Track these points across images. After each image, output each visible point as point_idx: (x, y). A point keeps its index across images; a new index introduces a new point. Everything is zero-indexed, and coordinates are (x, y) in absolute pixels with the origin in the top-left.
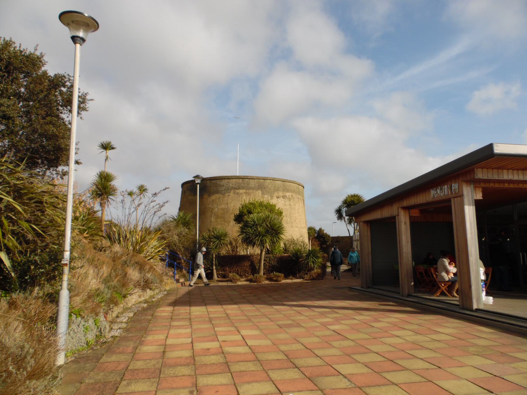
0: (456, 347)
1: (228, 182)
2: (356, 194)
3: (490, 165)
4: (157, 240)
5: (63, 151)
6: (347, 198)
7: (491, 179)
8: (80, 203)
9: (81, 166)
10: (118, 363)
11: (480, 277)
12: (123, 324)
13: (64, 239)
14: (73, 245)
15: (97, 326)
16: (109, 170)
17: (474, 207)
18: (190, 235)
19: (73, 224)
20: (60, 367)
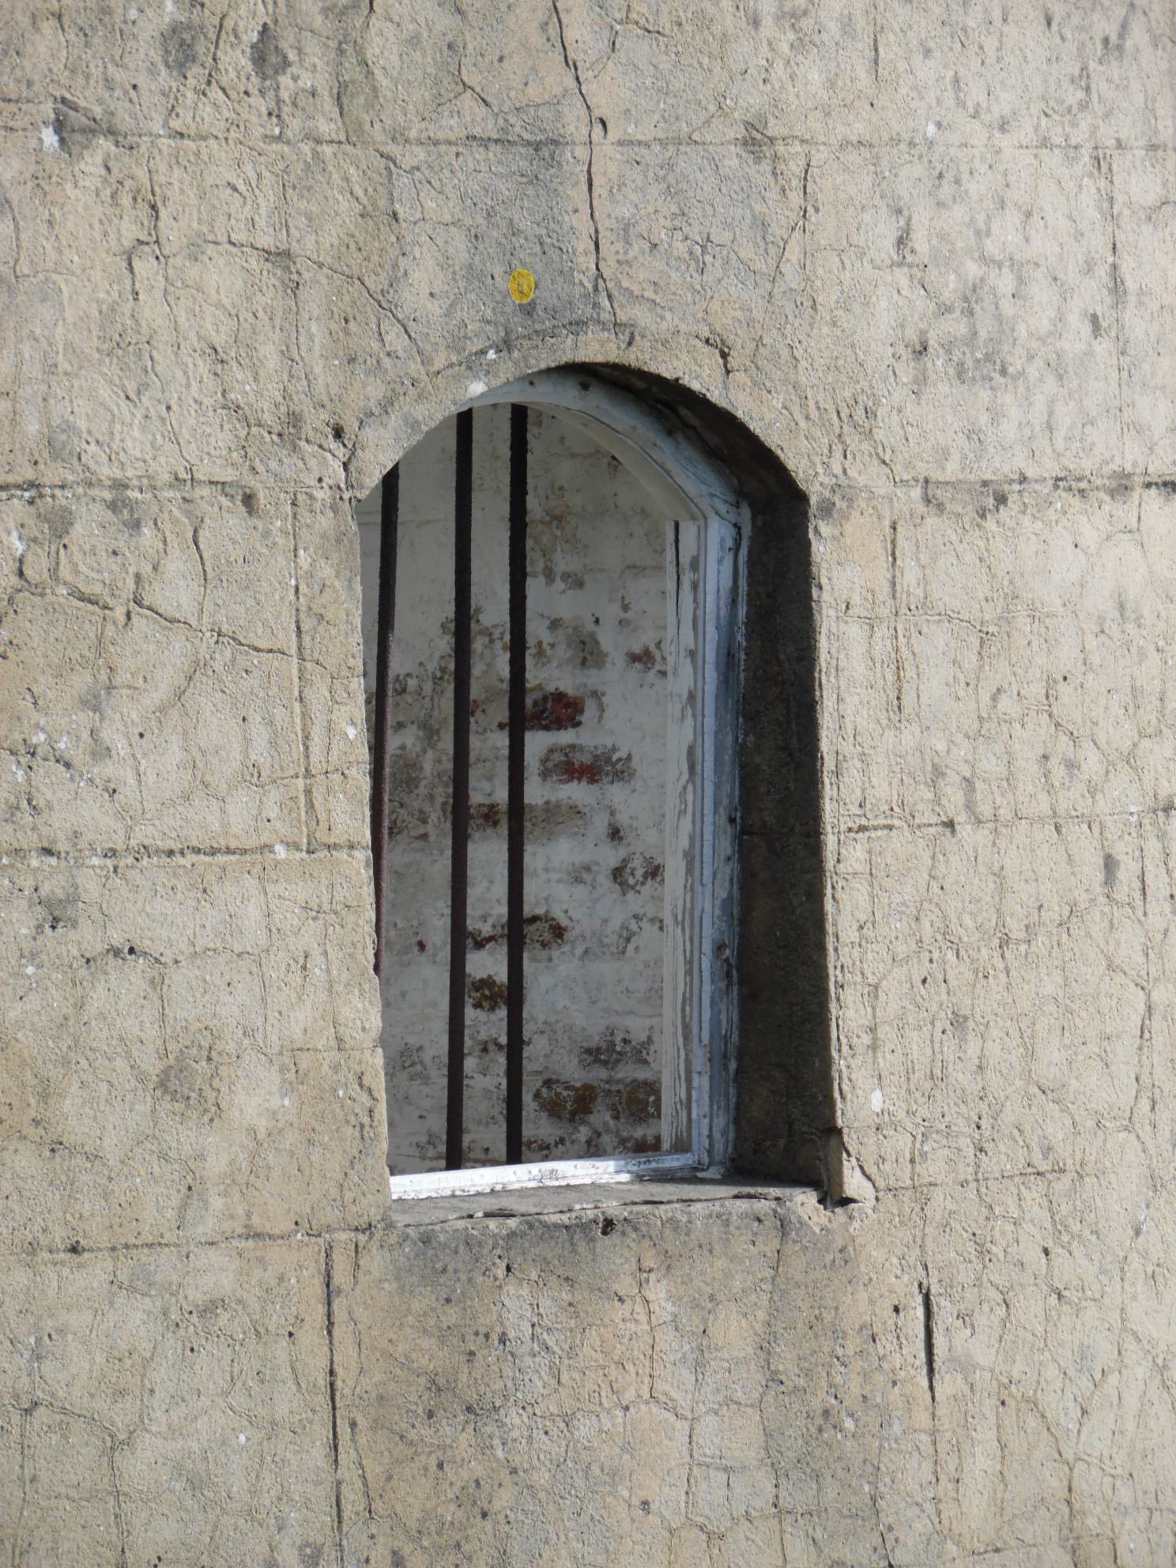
0: (212, 1244)
1: (577, 183)
2: (584, 783)
3: (684, 912)
4: (804, 1202)
5: (610, 758)
6: (733, 1160)
7: (827, 976)
8: (846, 1262)
9: (634, 754)
10: (951, 681)
11: (841, 1185)
12: (1124, 11)
13: (759, 523)
14: (932, 307)
15: (652, 920)
16: (494, 726)
17: (526, 801)
18: (610, 1329)
19: (642, 1074)
20: (873, 1090)
